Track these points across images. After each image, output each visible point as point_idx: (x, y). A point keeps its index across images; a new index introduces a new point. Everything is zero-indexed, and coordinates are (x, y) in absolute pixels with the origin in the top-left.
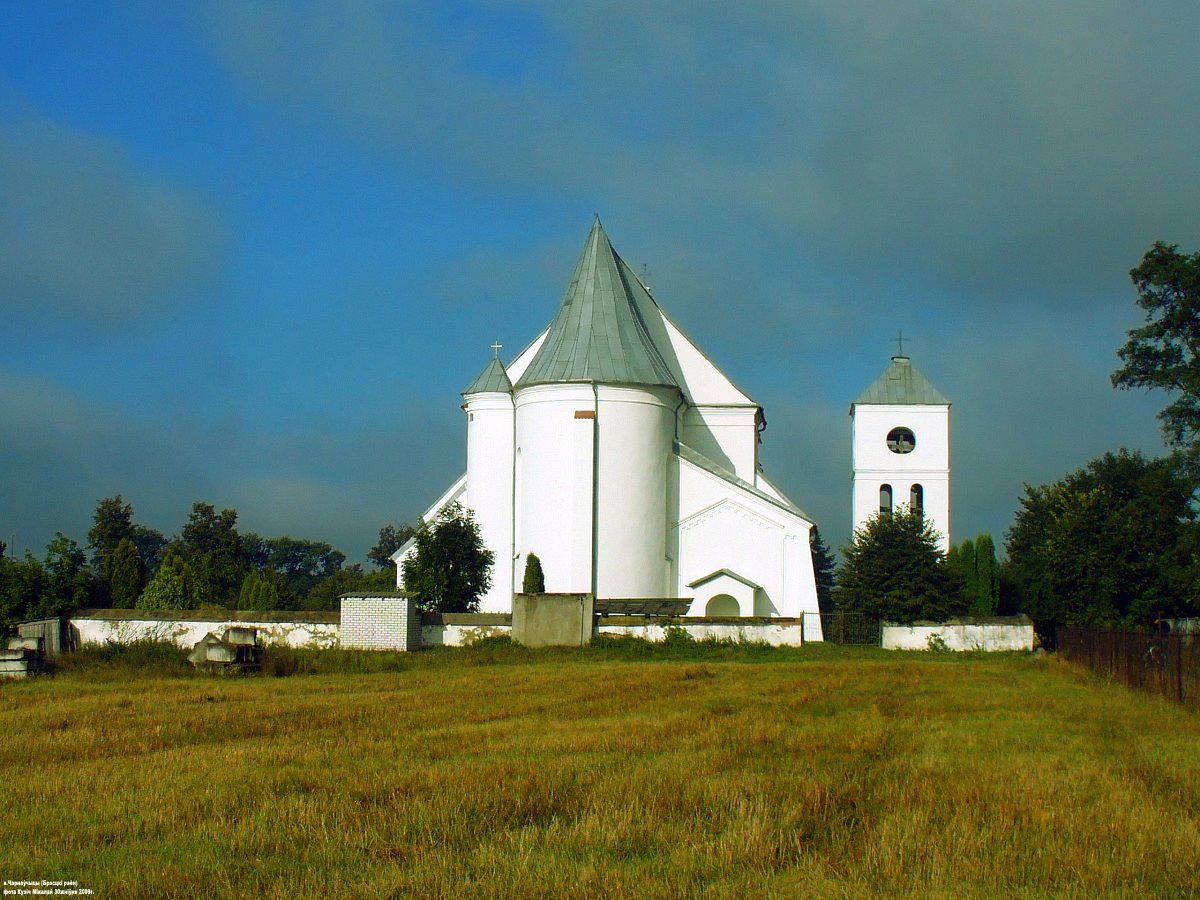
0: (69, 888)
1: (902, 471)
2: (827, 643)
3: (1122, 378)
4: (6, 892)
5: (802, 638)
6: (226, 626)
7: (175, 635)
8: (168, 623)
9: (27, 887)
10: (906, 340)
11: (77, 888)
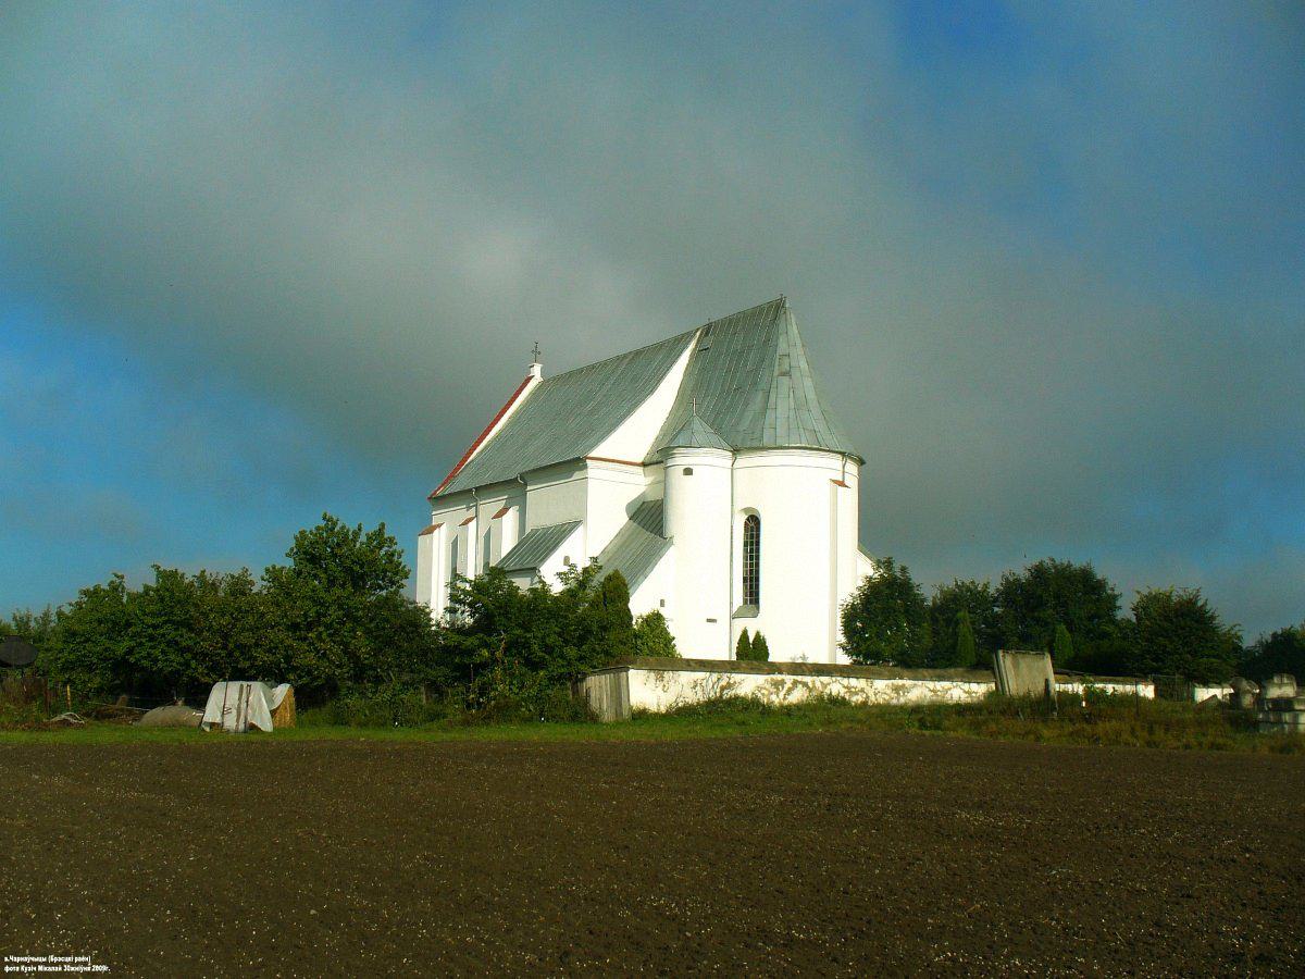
2: (1164, 703)
4: (7, 969)
6: (772, 680)
7: (723, 689)
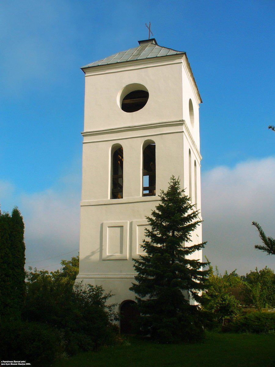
0: (23, 363)
3: (210, 263)
4: (2, 364)
8: (157, 235)
11: (25, 363)
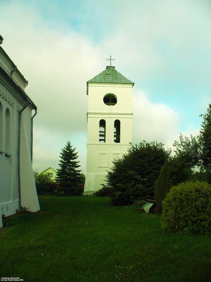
1: (110, 114)
4: (1, 280)
5: (20, 202)
9: (7, 279)
10: (113, 60)
11: (19, 279)
